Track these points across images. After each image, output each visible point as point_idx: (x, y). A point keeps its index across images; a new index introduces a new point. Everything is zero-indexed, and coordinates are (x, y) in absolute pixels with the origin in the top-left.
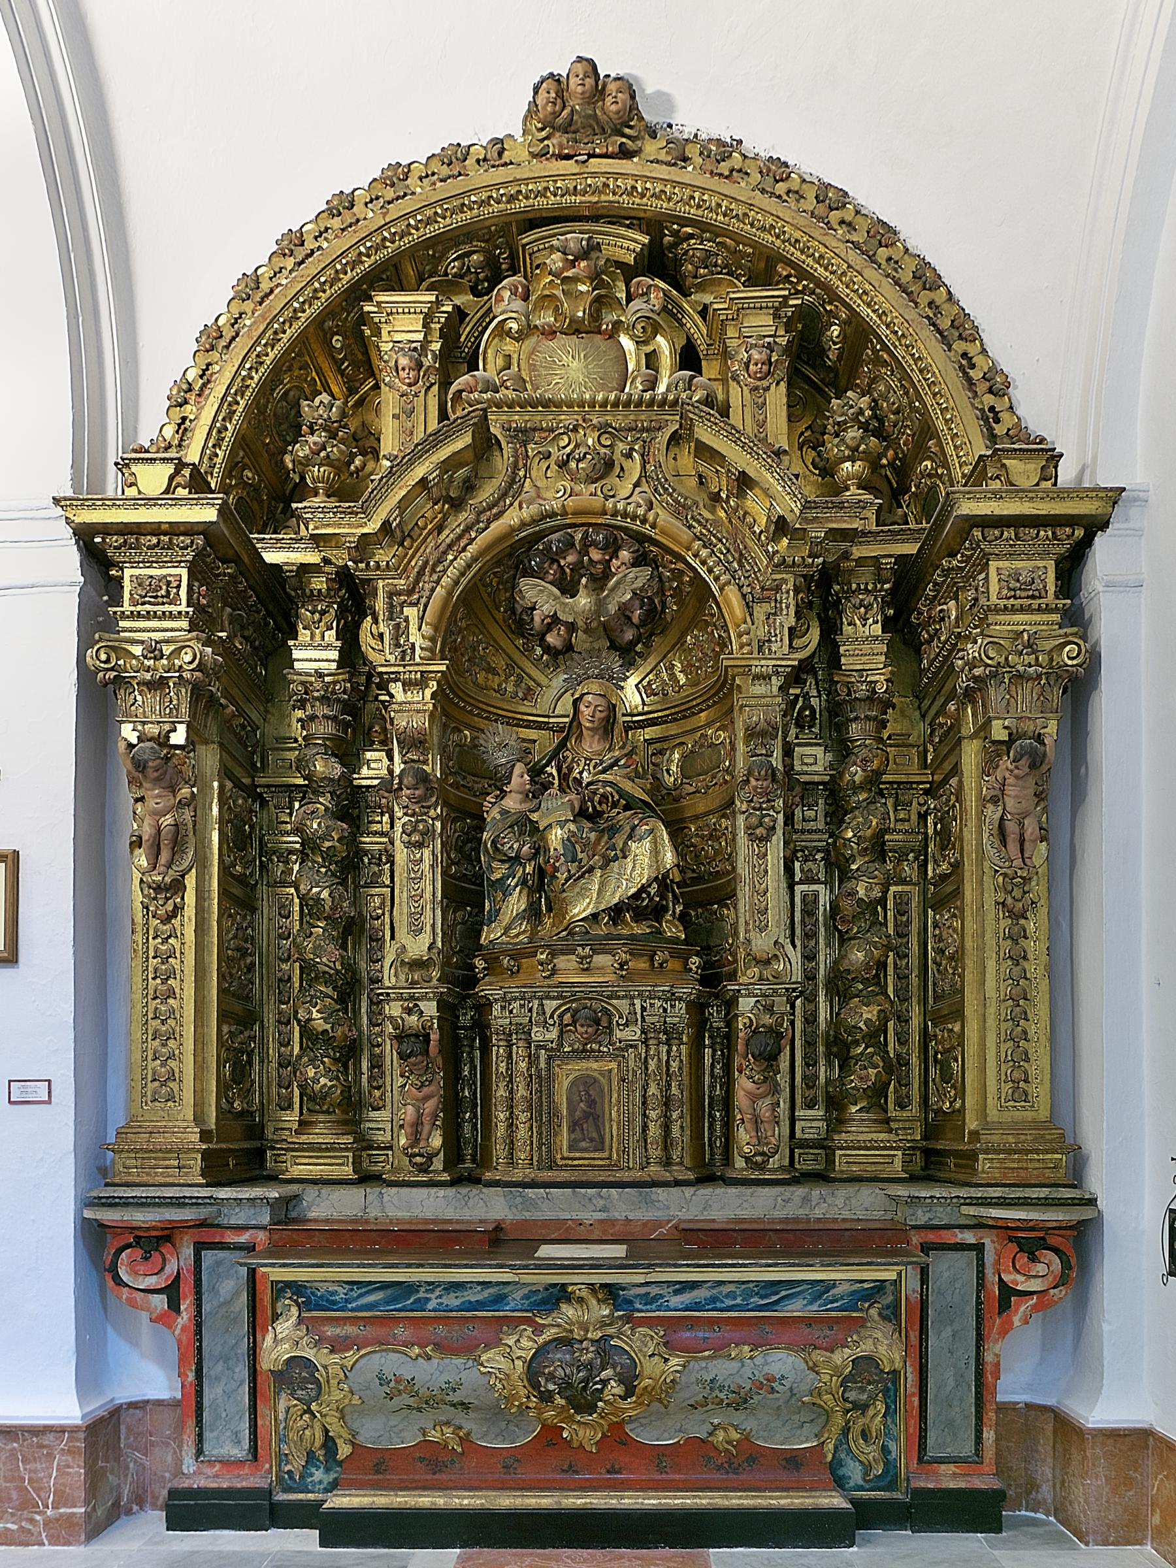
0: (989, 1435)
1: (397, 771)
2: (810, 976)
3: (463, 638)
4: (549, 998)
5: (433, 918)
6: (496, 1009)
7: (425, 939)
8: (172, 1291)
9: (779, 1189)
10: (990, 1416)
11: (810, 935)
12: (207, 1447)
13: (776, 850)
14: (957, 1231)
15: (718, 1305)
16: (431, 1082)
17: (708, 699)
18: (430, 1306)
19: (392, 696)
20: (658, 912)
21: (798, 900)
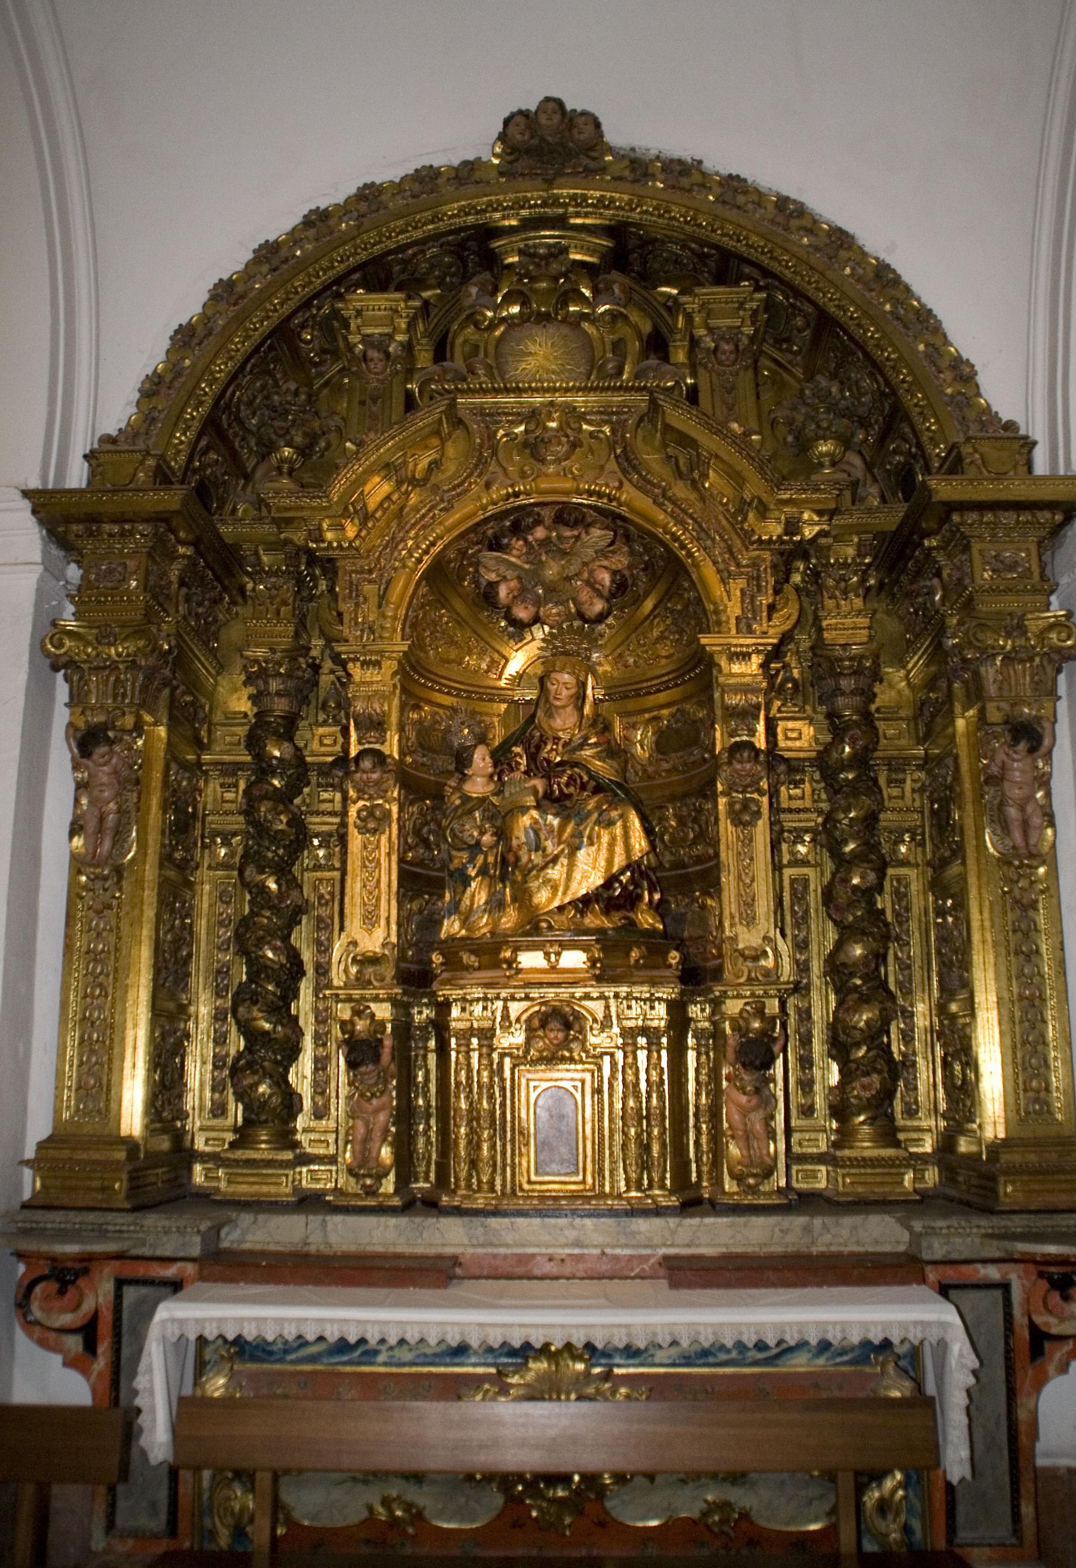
0: (1027, 1510)
1: (353, 753)
2: (803, 968)
3: (425, 615)
4: (513, 998)
5: (388, 908)
6: (455, 1012)
7: (379, 933)
8: (89, 1332)
9: (773, 1220)
10: (1027, 1486)
11: (802, 921)
12: (119, 1521)
13: (761, 832)
14: (979, 1266)
15: (711, 1360)
16: (382, 1093)
17: (684, 674)
18: (381, 1358)
19: (349, 675)
20: (630, 900)
21: (786, 883)
